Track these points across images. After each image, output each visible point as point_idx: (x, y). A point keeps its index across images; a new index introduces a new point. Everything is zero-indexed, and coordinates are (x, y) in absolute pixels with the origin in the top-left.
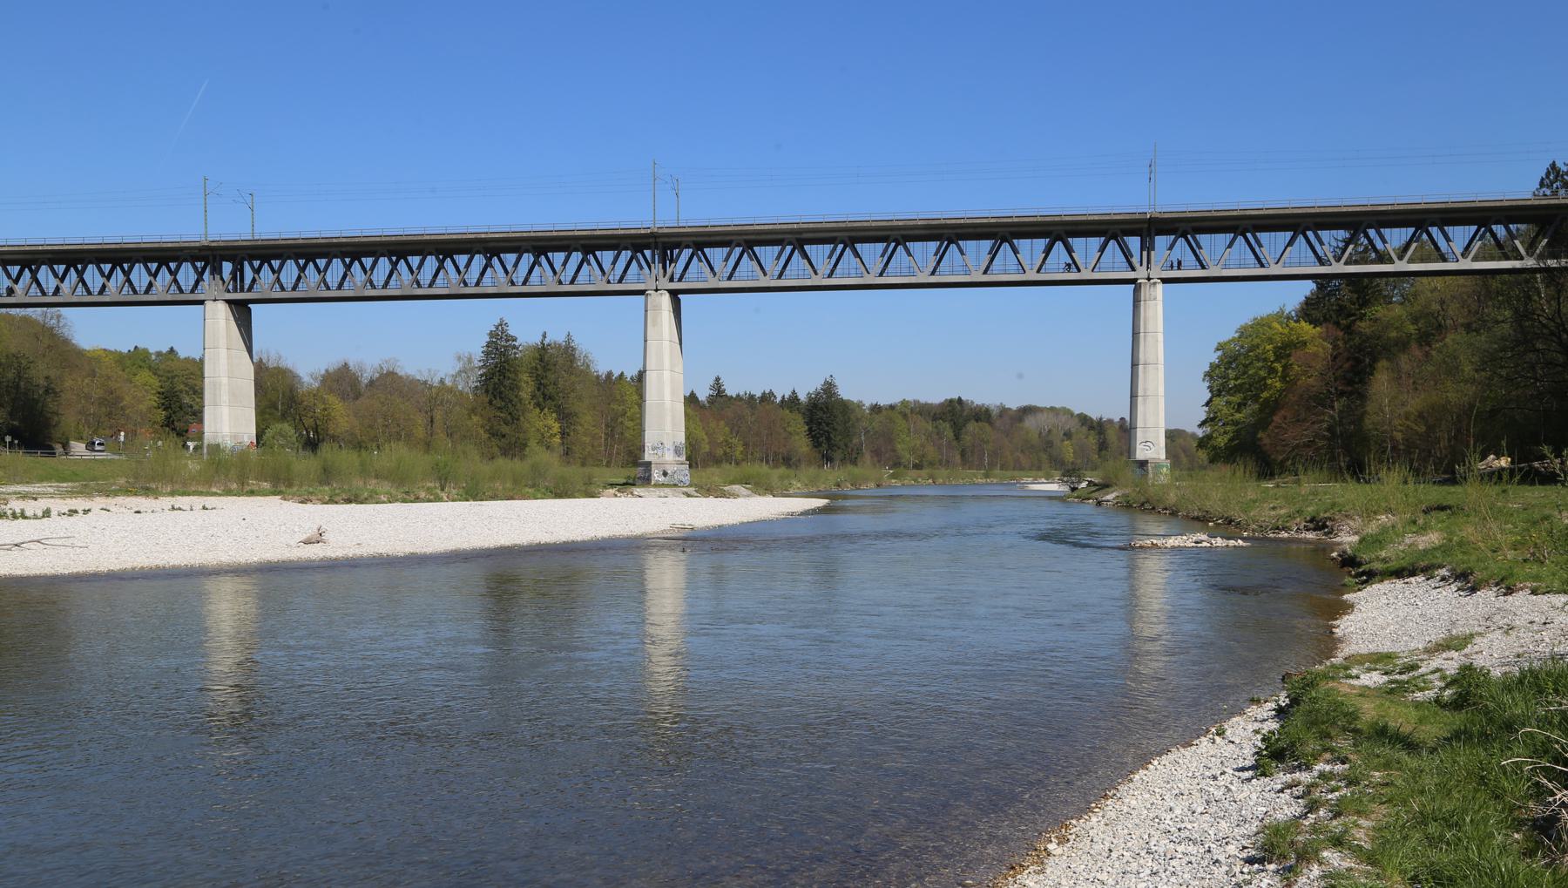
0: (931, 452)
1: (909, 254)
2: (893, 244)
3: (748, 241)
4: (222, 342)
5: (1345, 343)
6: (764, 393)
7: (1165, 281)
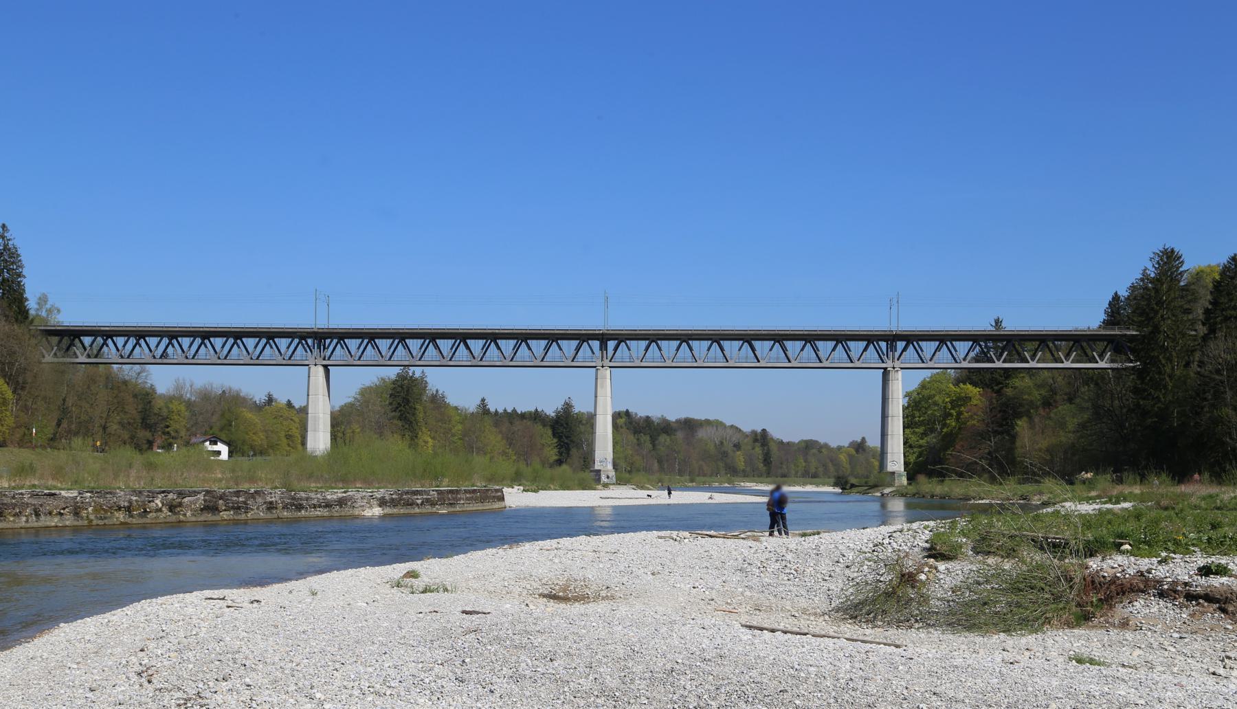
2: (489, 341)
5: (997, 401)
7: (901, 368)
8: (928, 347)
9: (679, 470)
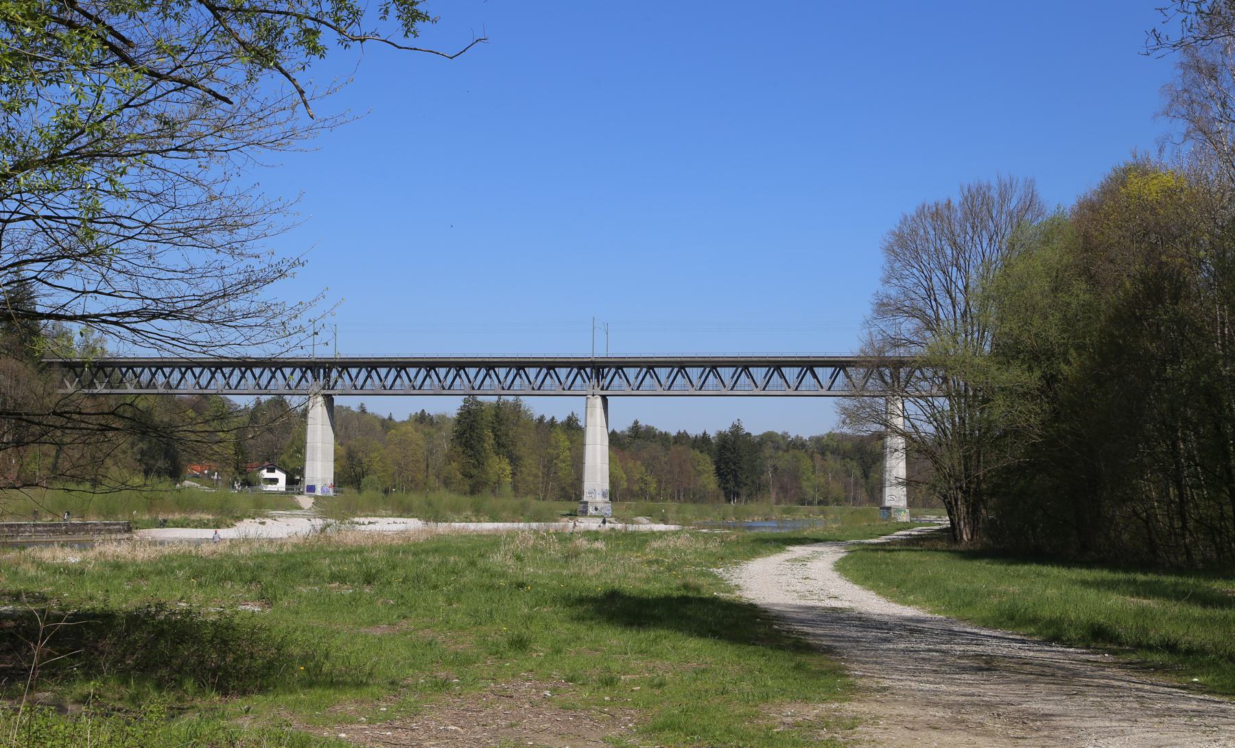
4: (319, 420)
6: (679, 433)
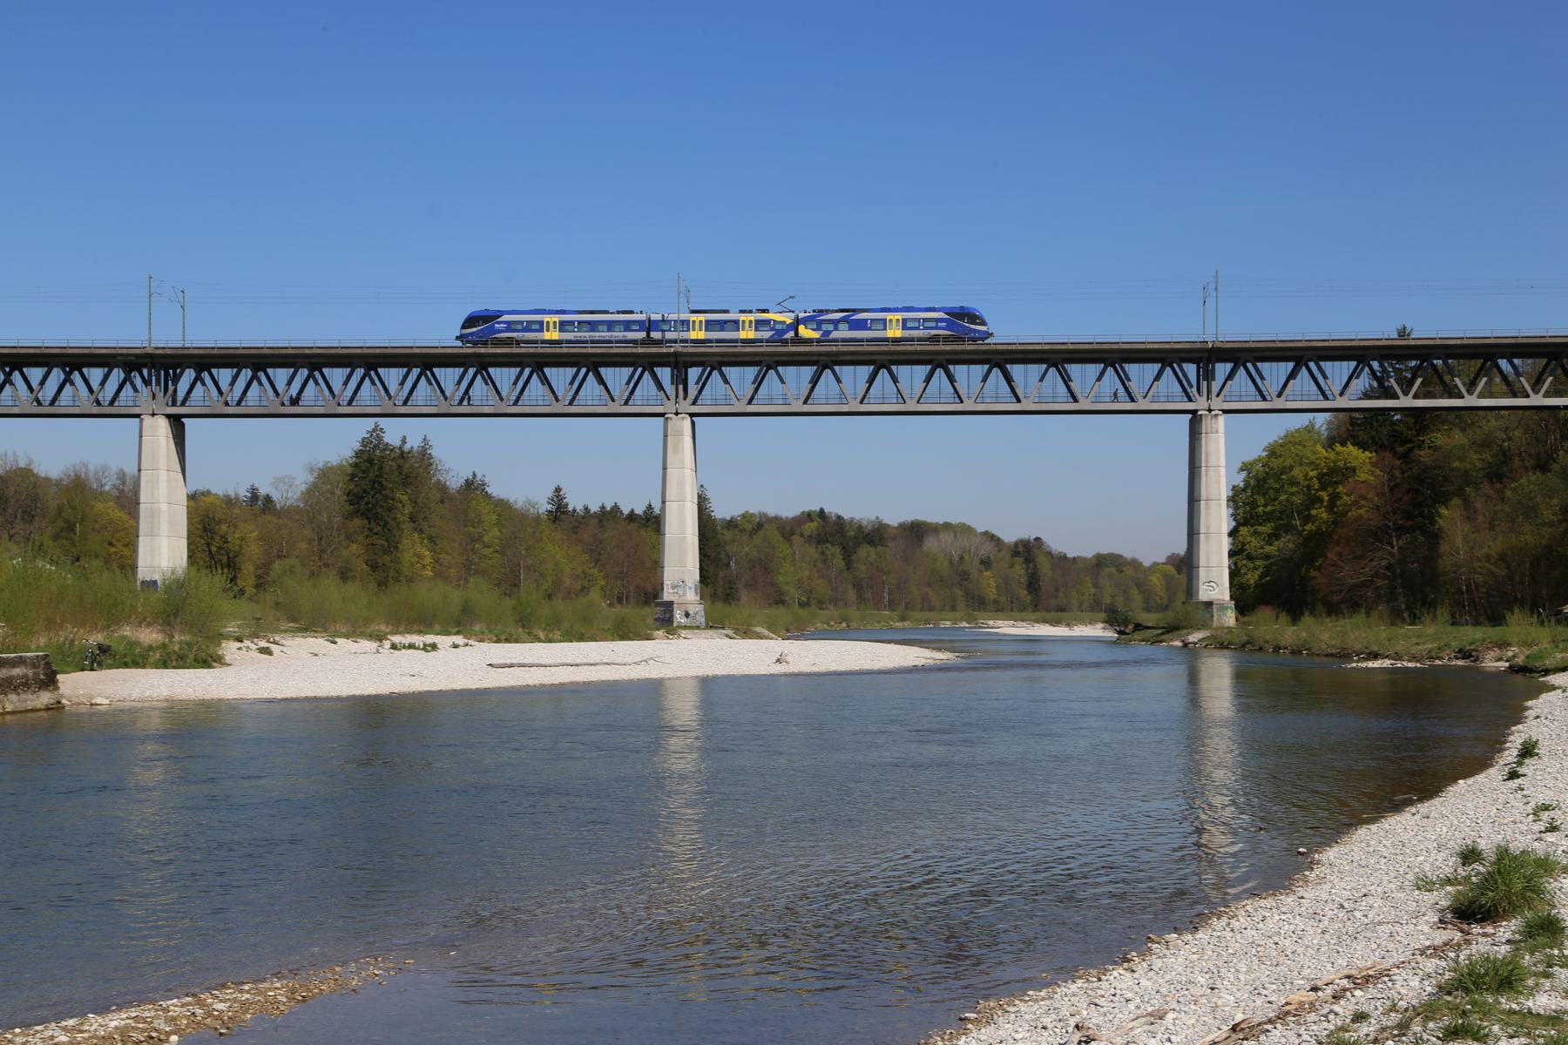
0: (822, 588)
1: (726, 381)
3: (258, 362)
4: (163, 463)
5: (1403, 473)
7: (1225, 412)
8: (1275, 372)
9: (890, 602)
